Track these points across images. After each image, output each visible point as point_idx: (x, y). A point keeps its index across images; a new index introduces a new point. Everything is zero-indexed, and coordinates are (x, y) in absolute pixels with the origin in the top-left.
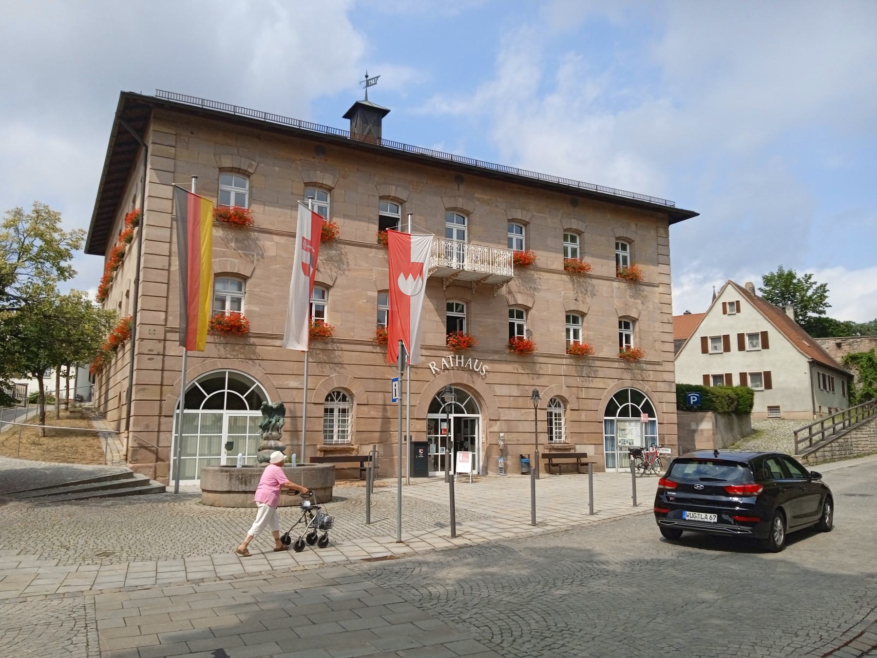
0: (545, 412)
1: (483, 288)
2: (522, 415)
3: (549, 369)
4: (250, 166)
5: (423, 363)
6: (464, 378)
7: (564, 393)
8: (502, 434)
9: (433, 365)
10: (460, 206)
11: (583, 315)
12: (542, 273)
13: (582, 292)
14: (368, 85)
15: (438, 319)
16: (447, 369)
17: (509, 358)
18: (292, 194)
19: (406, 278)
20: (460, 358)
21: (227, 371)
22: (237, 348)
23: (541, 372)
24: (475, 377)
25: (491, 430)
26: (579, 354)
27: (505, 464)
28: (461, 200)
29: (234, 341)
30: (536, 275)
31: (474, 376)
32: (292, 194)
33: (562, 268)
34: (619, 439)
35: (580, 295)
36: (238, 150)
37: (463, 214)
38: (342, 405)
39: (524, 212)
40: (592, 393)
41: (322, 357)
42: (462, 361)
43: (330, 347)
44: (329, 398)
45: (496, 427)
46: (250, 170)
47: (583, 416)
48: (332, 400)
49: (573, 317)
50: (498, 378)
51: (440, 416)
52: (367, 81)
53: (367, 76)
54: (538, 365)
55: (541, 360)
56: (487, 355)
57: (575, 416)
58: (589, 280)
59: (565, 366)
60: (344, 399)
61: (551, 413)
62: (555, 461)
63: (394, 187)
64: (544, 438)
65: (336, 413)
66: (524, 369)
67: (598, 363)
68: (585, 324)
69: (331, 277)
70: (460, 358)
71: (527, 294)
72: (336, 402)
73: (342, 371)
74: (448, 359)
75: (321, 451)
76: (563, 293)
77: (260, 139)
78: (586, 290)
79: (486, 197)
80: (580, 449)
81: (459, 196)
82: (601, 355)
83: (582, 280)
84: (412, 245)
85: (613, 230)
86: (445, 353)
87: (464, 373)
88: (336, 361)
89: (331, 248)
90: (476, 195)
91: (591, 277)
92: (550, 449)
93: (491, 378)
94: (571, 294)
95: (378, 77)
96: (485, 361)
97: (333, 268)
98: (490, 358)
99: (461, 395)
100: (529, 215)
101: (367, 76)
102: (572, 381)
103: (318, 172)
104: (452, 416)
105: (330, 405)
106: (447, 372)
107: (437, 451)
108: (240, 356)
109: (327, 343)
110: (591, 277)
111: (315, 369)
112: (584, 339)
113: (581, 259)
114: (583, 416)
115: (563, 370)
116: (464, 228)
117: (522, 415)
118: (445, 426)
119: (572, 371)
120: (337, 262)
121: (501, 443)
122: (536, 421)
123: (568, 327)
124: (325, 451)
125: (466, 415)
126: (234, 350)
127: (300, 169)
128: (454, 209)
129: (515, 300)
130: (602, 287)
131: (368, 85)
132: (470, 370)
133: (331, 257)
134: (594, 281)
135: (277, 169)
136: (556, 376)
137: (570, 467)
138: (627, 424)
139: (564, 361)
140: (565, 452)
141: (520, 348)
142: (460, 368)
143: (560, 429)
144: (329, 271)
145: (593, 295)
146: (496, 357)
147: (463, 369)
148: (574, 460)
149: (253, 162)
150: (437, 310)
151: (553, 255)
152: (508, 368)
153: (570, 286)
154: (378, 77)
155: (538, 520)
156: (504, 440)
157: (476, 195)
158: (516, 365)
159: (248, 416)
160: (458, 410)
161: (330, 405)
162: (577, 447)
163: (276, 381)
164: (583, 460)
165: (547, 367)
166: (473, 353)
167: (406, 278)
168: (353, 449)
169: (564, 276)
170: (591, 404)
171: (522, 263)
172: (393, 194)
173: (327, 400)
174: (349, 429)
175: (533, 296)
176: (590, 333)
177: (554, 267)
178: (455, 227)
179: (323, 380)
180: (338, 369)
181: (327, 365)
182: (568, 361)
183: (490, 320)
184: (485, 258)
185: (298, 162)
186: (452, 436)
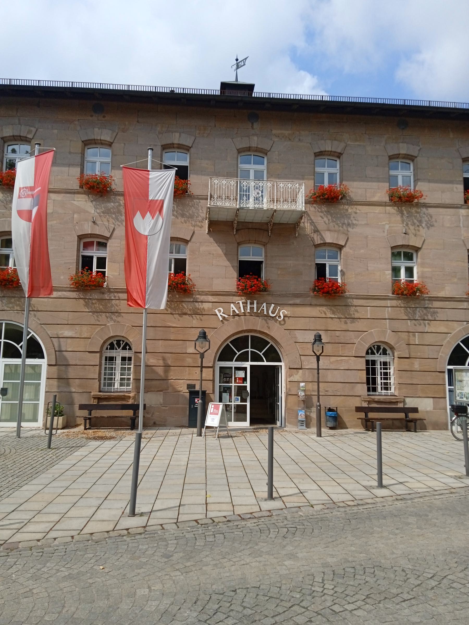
0: (364, 360)
1: (278, 230)
2: (331, 363)
3: (369, 313)
4: (30, 132)
5: (209, 310)
6: (258, 325)
7: (389, 338)
8: (302, 384)
9: (220, 311)
10: (254, 145)
11: (417, 249)
12: (358, 207)
13: (414, 224)
14: (238, 67)
15: (228, 263)
16: (238, 315)
17: (314, 301)
18: (70, 153)
19: (143, 217)
20: (252, 303)
21: (4, 322)
22: (13, 300)
23: (357, 315)
24: (271, 322)
25: (292, 379)
26: (409, 294)
27: (307, 417)
28: (255, 138)
29: (11, 295)
30: (350, 210)
31: (269, 321)
32: (70, 153)
33: (387, 199)
34: (458, 391)
35: (412, 228)
36: (19, 120)
37: (261, 152)
38: (383, 359)
39: (336, 143)
40: (429, 339)
41: (99, 306)
42: (255, 306)
43: (106, 296)
44: (370, 351)
45: (298, 376)
46: (30, 136)
47: (417, 365)
48: (373, 353)
49: (405, 253)
50: (301, 323)
51: (233, 364)
52: (237, 64)
53: (237, 60)
54: (353, 309)
55: (356, 302)
56: (284, 299)
57: (406, 364)
58: (424, 210)
59: (392, 308)
60: (385, 352)
61: (374, 362)
62: (371, 415)
63: (177, 135)
64: (362, 389)
65: (119, 361)
66: (334, 313)
67: (437, 304)
68: (419, 260)
69: (108, 228)
70: (252, 303)
71: (338, 231)
72: (378, 355)
73: (119, 319)
74: (239, 305)
75: (95, 398)
76: (387, 227)
77: (39, 106)
78: (420, 222)
79: (286, 133)
80: (410, 403)
81: (253, 135)
82: (442, 294)
83: (414, 210)
84: (150, 182)
85: (458, 151)
86: (236, 299)
87: (257, 318)
88: (113, 309)
89: (109, 202)
90: (274, 132)
91: (426, 206)
92: (369, 402)
93: (290, 323)
94: (399, 227)
95: (246, 59)
96: (283, 305)
97: (111, 220)
98: (291, 302)
99: (259, 342)
100: (342, 145)
101: (237, 60)
102: (398, 325)
103: (96, 129)
104: (247, 365)
105: (112, 353)
106: (237, 318)
107: (230, 401)
108: (16, 308)
109: (103, 293)
110: (426, 206)
111: (92, 319)
112: (418, 277)
113: (415, 187)
114: (417, 365)
115: (387, 313)
116: (263, 167)
117: (331, 363)
118: (241, 374)
119: (401, 314)
120: (114, 213)
121: (302, 394)
122: (318, 369)
123: (396, 264)
124: (99, 399)
125: (265, 363)
126: (11, 303)
127: (78, 128)
128: (249, 149)
129: (322, 238)
130: (445, 217)
131: (238, 67)
132: (265, 316)
133: (109, 210)
134: (431, 210)
135: (55, 131)
136: (378, 321)
137: (397, 423)
138: (464, 374)
139: (389, 303)
140: (390, 406)
141: (327, 289)
142: (252, 313)
143: (122, 379)
144: (106, 223)
145: (430, 226)
146: (298, 301)
147: (257, 315)
148: (401, 415)
149: (32, 129)
150: (225, 254)
151: (375, 185)
152: (308, 311)
153: (399, 218)
154: (246, 59)
155: (137, 511)
156: (304, 391)
157: (274, 132)
158: (324, 309)
159: (233, 366)
160: (256, 358)
161: (371, 358)
162: (408, 400)
163: (52, 331)
164: (412, 416)
165: (367, 311)
166: (270, 298)
167: (143, 217)
168: (129, 397)
169: (388, 208)
170: (428, 352)
171: (328, 198)
172: (176, 142)
173: (367, 353)
174: (131, 377)
175: (346, 234)
176: (426, 270)
177: (376, 199)
178: (252, 168)
179: (99, 328)
180: (114, 318)
181: (104, 314)
182: (394, 303)
183: (290, 262)
184: (272, 191)
185: (77, 123)
186: (248, 384)
